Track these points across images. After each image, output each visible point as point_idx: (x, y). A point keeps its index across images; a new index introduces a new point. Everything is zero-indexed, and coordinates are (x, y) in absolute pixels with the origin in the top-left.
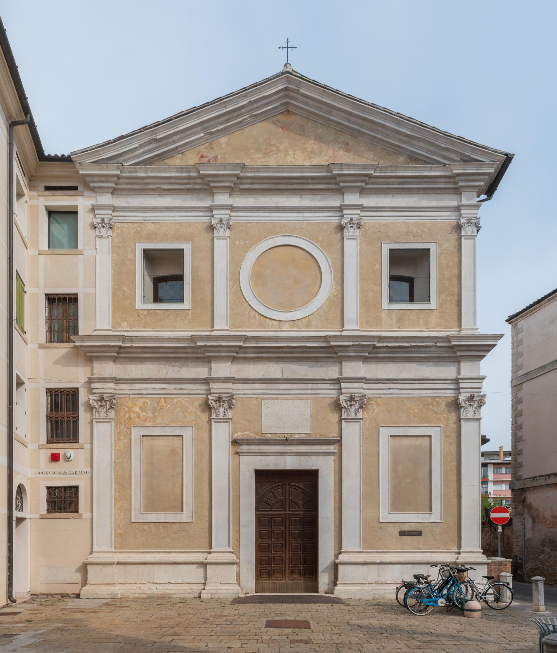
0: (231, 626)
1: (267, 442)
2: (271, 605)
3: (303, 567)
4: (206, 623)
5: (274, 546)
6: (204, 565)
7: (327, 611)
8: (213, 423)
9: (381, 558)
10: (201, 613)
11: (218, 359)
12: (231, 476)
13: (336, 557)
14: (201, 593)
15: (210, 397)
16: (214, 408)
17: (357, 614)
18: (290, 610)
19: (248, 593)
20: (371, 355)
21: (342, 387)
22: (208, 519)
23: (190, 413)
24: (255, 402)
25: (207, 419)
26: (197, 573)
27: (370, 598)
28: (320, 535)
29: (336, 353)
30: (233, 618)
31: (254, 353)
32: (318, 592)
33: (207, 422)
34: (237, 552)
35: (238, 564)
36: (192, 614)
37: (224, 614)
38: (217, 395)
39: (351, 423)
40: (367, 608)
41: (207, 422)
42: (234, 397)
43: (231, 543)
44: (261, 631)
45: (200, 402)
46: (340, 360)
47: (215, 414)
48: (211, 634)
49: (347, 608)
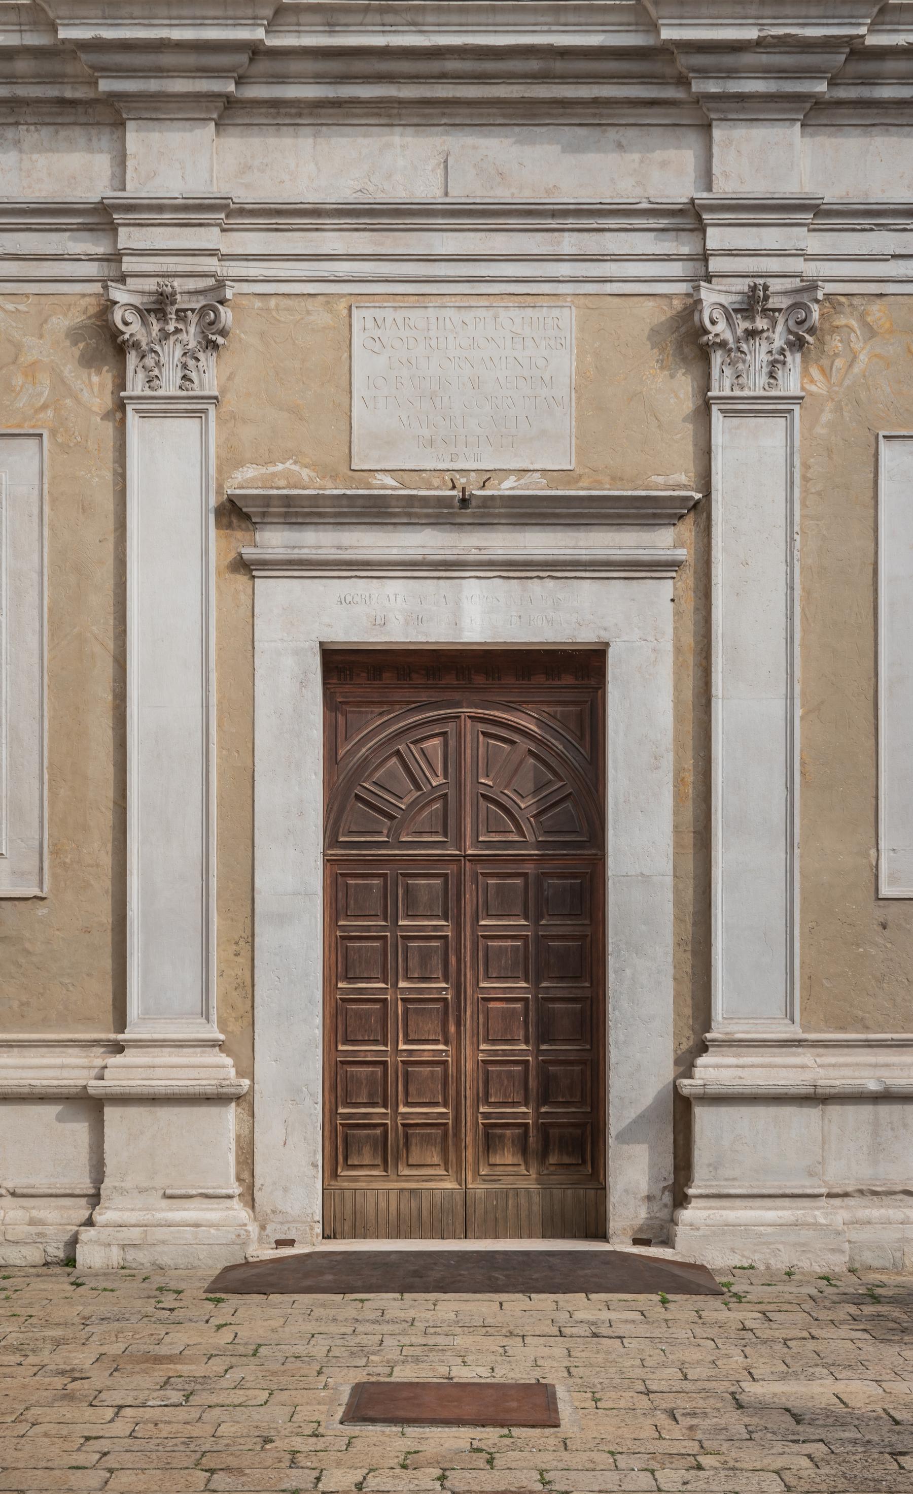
0: (182, 1414)
1: (375, 511)
2: (387, 1300)
3: (539, 1115)
4: (69, 1397)
5: (406, 1011)
6: (90, 1105)
7: (642, 1330)
8: (132, 418)
9: (883, 1073)
10: (58, 1343)
11: (157, 108)
12: (214, 676)
13: (685, 1064)
14: (74, 1242)
15: (119, 295)
16: (136, 345)
17: (778, 1347)
18: (469, 1328)
19: (291, 1243)
20: (843, 93)
21: (711, 244)
22: (108, 884)
23: (32, 370)
24: (320, 317)
25: (108, 402)
26: (51, 1148)
27: (838, 1263)
28: (611, 962)
29: (683, 81)
30: (199, 1370)
31: (319, 78)
32: (603, 1236)
33: (106, 416)
34: (240, 1043)
35: (242, 1099)
36: (17, 1349)
37: (164, 1350)
38: (150, 285)
39: (752, 422)
40: (823, 1315)
41: (106, 416)
42: (229, 294)
43: (214, 1002)
44: (320, 1443)
45: (77, 318)
46: (704, 119)
47: (141, 375)
48: (80, 1459)
49: (734, 1316)
